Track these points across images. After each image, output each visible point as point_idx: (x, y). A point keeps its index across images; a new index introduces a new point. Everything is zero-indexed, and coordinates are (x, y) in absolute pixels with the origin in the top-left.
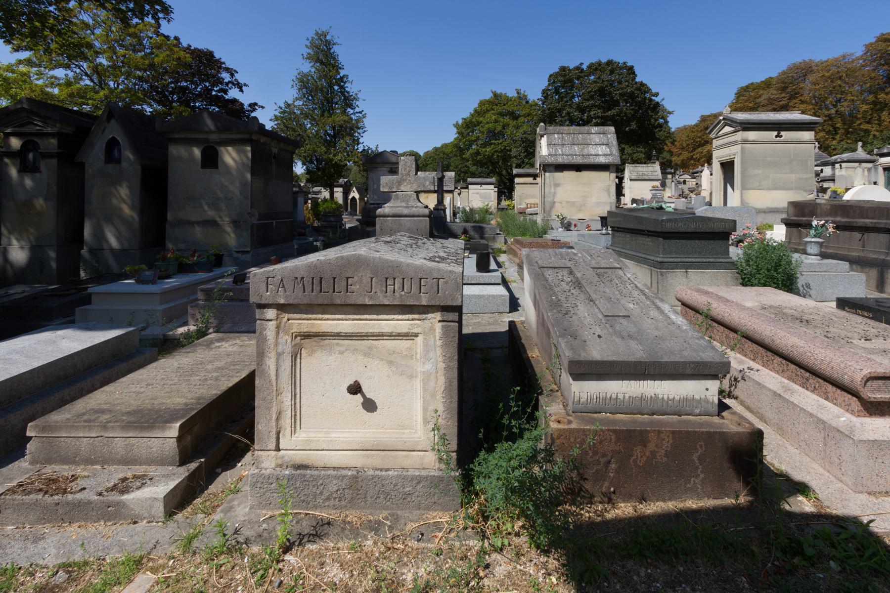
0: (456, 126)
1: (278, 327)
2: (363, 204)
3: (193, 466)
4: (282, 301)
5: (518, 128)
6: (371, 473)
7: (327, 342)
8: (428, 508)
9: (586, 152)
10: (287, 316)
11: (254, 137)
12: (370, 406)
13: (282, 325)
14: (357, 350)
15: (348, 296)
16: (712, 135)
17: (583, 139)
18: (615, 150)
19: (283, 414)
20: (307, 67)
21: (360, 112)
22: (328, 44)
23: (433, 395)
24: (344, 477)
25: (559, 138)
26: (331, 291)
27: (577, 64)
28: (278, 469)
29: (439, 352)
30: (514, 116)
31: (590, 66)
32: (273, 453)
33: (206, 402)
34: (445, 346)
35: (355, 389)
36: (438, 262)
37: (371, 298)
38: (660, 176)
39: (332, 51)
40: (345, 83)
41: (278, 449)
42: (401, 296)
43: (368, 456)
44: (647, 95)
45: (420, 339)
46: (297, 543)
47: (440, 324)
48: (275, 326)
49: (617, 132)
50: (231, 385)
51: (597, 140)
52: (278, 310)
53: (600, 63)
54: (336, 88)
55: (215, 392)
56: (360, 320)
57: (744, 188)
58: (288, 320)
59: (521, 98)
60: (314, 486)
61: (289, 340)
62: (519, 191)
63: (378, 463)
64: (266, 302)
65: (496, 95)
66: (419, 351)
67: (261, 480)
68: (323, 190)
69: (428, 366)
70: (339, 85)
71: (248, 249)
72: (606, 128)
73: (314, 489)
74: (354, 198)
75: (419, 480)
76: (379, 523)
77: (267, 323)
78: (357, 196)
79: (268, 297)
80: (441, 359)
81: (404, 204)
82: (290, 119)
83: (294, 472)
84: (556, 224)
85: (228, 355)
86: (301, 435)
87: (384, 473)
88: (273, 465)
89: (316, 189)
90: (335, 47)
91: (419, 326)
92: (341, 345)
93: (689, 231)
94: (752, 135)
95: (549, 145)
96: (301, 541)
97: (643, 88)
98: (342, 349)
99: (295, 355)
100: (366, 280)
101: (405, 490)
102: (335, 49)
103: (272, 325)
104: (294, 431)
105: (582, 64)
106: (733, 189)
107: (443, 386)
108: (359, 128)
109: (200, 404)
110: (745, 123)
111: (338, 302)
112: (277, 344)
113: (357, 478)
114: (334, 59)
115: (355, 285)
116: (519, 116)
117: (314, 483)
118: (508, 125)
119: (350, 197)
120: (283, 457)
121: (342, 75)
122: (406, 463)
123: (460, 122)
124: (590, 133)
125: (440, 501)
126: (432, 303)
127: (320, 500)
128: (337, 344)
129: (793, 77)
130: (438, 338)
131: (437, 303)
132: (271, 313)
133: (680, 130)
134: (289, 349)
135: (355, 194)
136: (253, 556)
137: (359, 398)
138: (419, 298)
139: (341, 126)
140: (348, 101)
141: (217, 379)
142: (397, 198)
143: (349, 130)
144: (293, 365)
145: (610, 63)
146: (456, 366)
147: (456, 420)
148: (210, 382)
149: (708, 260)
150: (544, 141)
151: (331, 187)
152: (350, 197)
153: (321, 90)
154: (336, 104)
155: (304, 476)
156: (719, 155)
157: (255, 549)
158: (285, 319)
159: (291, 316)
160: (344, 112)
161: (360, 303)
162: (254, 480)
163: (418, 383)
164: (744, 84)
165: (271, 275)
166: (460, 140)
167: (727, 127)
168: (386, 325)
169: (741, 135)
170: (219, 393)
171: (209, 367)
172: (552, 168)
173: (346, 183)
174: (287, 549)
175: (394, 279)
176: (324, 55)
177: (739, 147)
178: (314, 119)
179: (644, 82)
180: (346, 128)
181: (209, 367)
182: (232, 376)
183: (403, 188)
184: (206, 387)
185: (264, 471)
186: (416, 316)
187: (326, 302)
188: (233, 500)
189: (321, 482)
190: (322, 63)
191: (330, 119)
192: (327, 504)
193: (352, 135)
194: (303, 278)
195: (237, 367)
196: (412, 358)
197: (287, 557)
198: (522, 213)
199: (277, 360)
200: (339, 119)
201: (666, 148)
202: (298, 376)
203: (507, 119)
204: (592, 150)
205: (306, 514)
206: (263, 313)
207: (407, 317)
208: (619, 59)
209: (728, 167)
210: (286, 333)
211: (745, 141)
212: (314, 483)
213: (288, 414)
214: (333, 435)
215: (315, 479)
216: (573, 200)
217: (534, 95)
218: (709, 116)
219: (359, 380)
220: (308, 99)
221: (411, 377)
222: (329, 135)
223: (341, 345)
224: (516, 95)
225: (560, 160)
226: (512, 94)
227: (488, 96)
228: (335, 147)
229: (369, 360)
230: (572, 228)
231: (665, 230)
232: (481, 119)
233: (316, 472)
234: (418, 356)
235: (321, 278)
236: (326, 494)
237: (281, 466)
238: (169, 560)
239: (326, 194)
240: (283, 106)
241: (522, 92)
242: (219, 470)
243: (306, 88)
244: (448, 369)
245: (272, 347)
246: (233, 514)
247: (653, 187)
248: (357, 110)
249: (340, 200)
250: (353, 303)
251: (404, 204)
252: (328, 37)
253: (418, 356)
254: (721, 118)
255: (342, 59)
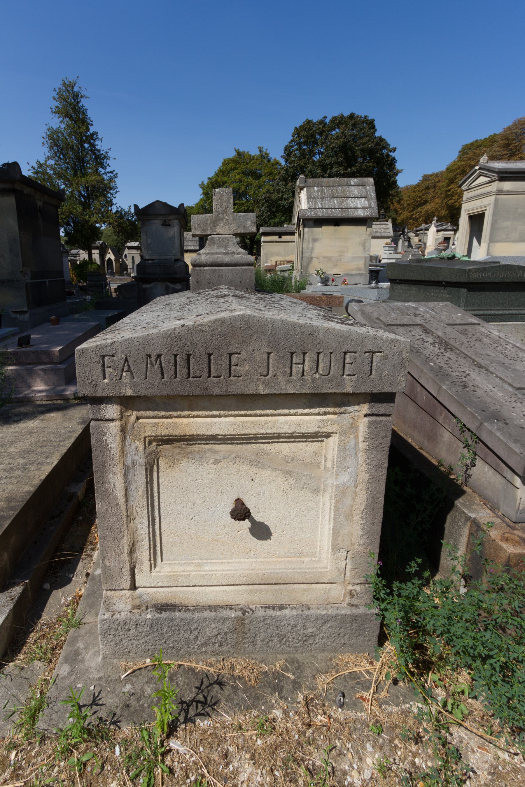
0: (202, 186)
1: (123, 430)
2: (118, 265)
3: (17, 590)
4: (129, 392)
5: (260, 187)
6: (261, 613)
7: (195, 447)
8: (335, 650)
9: (345, 205)
10: (135, 414)
11: (17, 187)
12: (261, 531)
13: (130, 426)
14: (239, 457)
15: (232, 383)
16: (464, 187)
17: (343, 192)
18: (374, 203)
19: (138, 546)
20: (57, 123)
21: (111, 172)
22: (77, 96)
23: (349, 516)
24: (225, 619)
25: (318, 191)
26: (206, 375)
27: (320, 118)
28: (136, 611)
29: (361, 458)
30: (256, 176)
31: (334, 119)
32: (128, 593)
33: (19, 505)
34: (371, 450)
35: (241, 512)
36: (352, 325)
37: (267, 384)
38: (392, 234)
39: (81, 104)
40: (95, 140)
41: (134, 587)
42: (314, 379)
43: (255, 592)
44: (385, 151)
45: (333, 442)
46: (182, 719)
47: (367, 419)
48: (118, 429)
49: (376, 184)
50: (43, 477)
51: (356, 192)
52: (121, 404)
53: (342, 117)
54: (86, 145)
55: (26, 488)
56: (246, 416)
57: (492, 240)
58: (138, 418)
59: (264, 156)
60: (186, 631)
61: (141, 447)
62: (265, 249)
63: (270, 599)
64: (105, 394)
65: (239, 154)
66: (330, 457)
67: (115, 626)
68: (81, 251)
69: (344, 478)
70: (89, 143)
71: (25, 309)
72: (366, 179)
73: (187, 635)
74: (109, 259)
75: (326, 620)
76: (277, 675)
77: (106, 424)
78: (113, 257)
79: (106, 385)
80: (363, 468)
81: (222, 250)
82: (44, 179)
83: (158, 615)
84: (316, 279)
85: (31, 433)
86: (164, 569)
87: (278, 613)
88: (129, 607)
89: (74, 251)
90: (82, 100)
91: (333, 422)
92: (217, 452)
93: (496, 281)
94: (507, 186)
95: (309, 198)
96: (187, 713)
97: (381, 143)
98: (218, 457)
99: (151, 467)
100: (260, 357)
101: (307, 632)
102: (84, 102)
103: (114, 427)
104: (153, 565)
105: (325, 117)
106: (479, 243)
107: (364, 504)
108: (111, 189)
109: (11, 508)
110: (502, 173)
111: (217, 391)
112: (123, 454)
113: (243, 619)
114: (84, 114)
115: (242, 364)
116: (261, 176)
117: (186, 627)
118: (251, 184)
119: (107, 259)
120: (141, 596)
121: (91, 131)
122: (306, 598)
123: (206, 182)
124: (349, 185)
125: (351, 643)
126: (362, 389)
127: (194, 646)
128: (211, 451)
129: (516, 133)
130: (361, 439)
131: (369, 390)
132: (112, 411)
133: (407, 188)
134: (141, 459)
135: (110, 255)
136: (126, 743)
137: (247, 523)
138: (341, 383)
139: (93, 186)
140: (100, 160)
141: (25, 468)
142: (213, 242)
143: (102, 190)
144: (149, 483)
145: (352, 116)
146: (385, 477)
147: (378, 545)
148: (18, 473)
149: (510, 312)
150: (303, 195)
151: (89, 249)
152: (107, 259)
153: (72, 148)
154: (88, 163)
155: (172, 620)
156: (467, 208)
157: (126, 730)
158: (133, 418)
159: (141, 413)
160: (96, 172)
161: (250, 392)
162: (106, 627)
163: (326, 501)
164: (469, 141)
165: (108, 351)
166: (206, 202)
167: (481, 178)
168: (286, 422)
169: (496, 186)
170: (32, 489)
171: (12, 450)
172: (311, 223)
173: (101, 245)
174: (171, 730)
175: (304, 354)
176: (72, 108)
177: (493, 198)
178: (68, 180)
179: (383, 137)
180: (99, 188)
181: (12, 450)
182: (42, 463)
183: (219, 230)
184: (14, 481)
185: (117, 616)
186: (331, 410)
187: (197, 393)
188: (75, 639)
189: (195, 626)
190: (70, 117)
191: (83, 180)
192: (203, 650)
193: (105, 196)
194: (159, 356)
195: (44, 449)
196: (318, 466)
197: (174, 744)
198: (269, 270)
199: (126, 475)
200: (92, 179)
201: (392, 207)
202: (156, 494)
203: (250, 179)
204: (351, 203)
205: (180, 666)
206: (99, 411)
207: (317, 410)
208: (360, 112)
209: (477, 220)
210: (136, 438)
211: (500, 192)
212: (186, 627)
213: (144, 545)
214: (207, 568)
215: (187, 623)
216: (330, 255)
217: (277, 154)
218: (431, 175)
219: (242, 497)
220: (59, 157)
221: (316, 491)
222: (83, 196)
223: (217, 452)
224: (258, 153)
225: (320, 214)
226: (254, 152)
227: (232, 154)
228: (89, 208)
229: (257, 470)
230: (330, 282)
231: (471, 280)
232: (226, 179)
233: (188, 615)
234: (329, 464)
235: (189, 355)
236: (202, 639)
237: (139, 607)
238: (9, 751)
239: (83, 255)
240: (36, 166)
241: (264, 150)
242: (47, 586)
243: (57, 146)
244: (372, 481)
245: (117, 458)
246: (81, 666)
247: (387, 244)
248: (108, 169)
249: (98, 262)
250: (239, 392)
251: (222, 250)
252: (76, 89)
253: (329, 464)
254: (477, 168)
255: (90, 114)
